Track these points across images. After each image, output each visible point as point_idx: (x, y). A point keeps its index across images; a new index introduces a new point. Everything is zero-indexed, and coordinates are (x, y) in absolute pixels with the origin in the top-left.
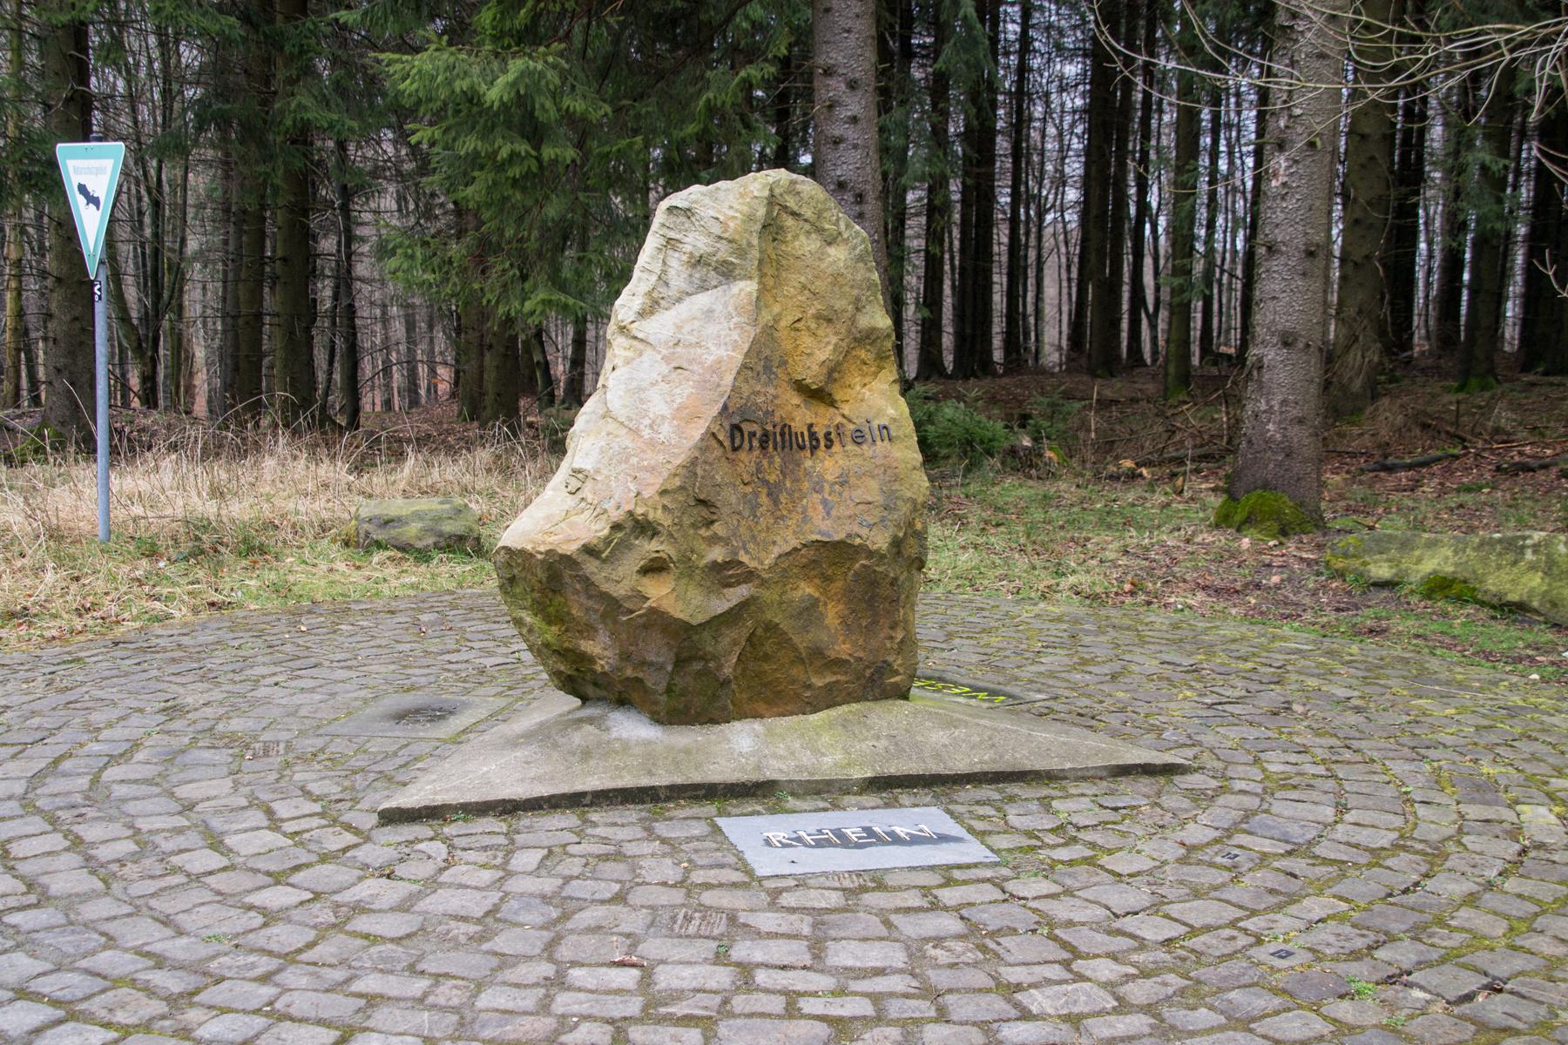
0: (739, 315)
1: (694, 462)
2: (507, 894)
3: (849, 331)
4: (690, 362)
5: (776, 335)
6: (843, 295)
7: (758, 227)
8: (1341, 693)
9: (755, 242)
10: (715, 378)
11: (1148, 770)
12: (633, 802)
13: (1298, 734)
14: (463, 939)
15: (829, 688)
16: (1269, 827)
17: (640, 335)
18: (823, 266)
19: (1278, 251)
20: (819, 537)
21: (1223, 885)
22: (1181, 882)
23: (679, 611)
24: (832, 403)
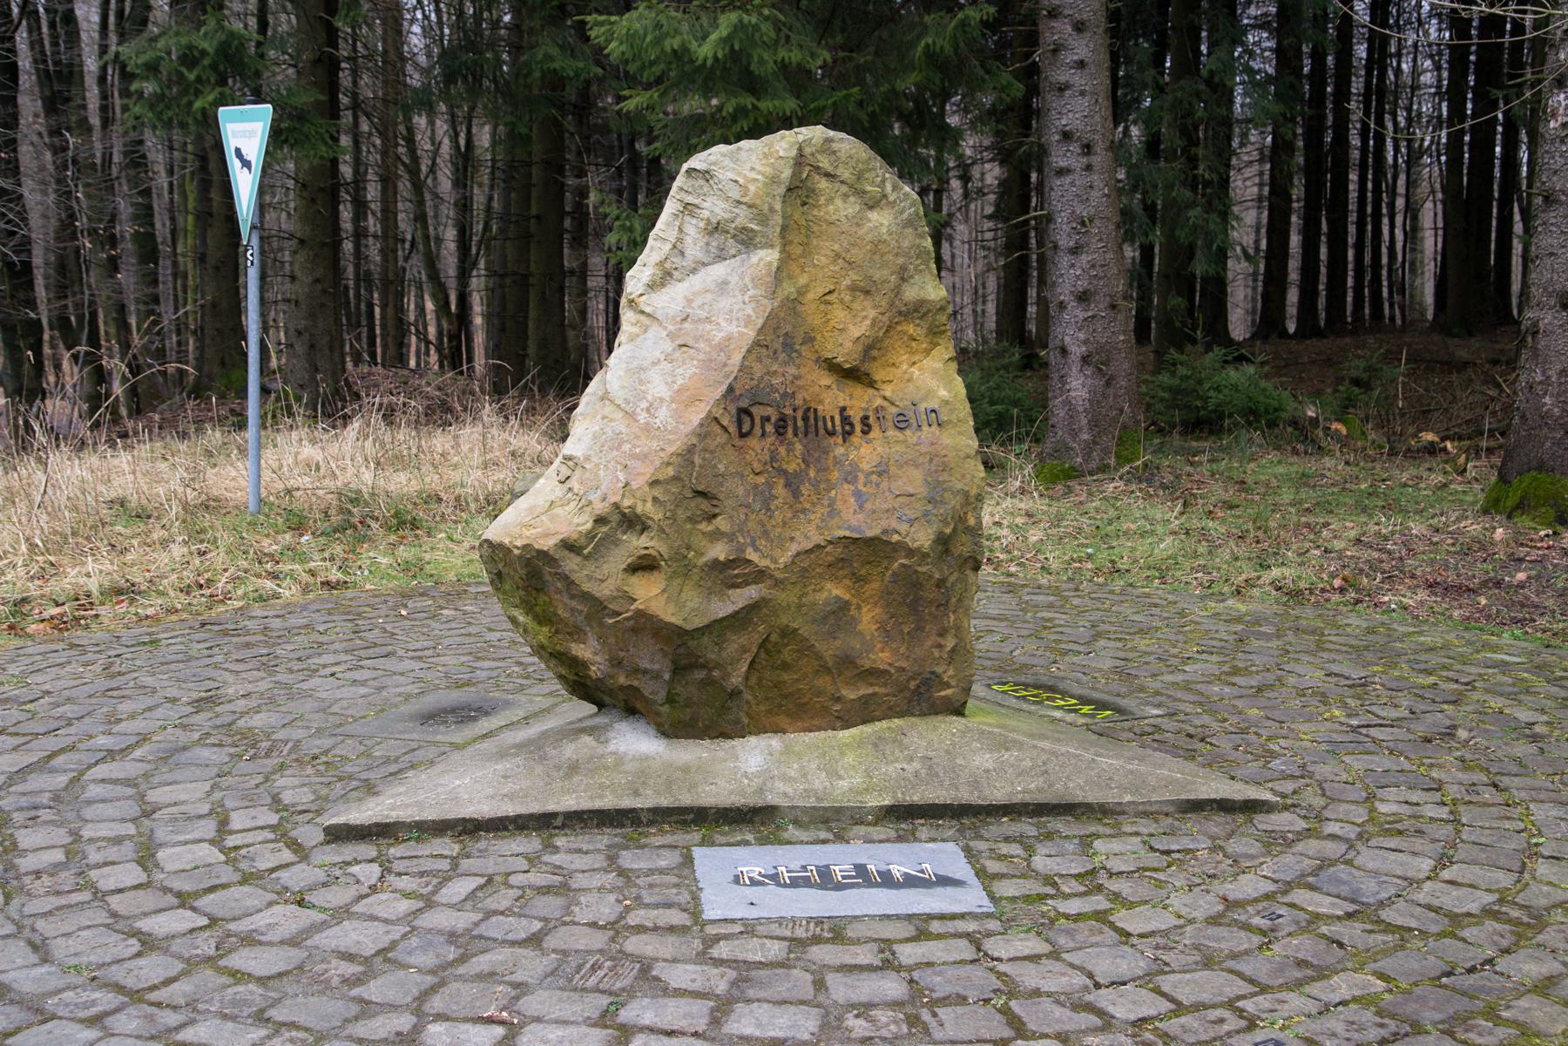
0: (755, 287)
1: (691, 450)
2: (414, 928)
3: (892, 304)
4: (697, 340)
5: (800, 308)
6: (884, 265)
7: (782, 190)
8: (1524, 715)
9: (778, 206)
10: (722, 357)
11: (1225, 806)
12: (611, 825)
13: (1440, 766)
14: (335, 981)
15: (865, 701)
16: (1340, 882)
17: (648, 310)
18: (860, 233)
19: (1557, 201)
20: (847, 534)
21: (1247, 952)
22: (1197, 947)
23: (669, 614)
24: (871, 384)
